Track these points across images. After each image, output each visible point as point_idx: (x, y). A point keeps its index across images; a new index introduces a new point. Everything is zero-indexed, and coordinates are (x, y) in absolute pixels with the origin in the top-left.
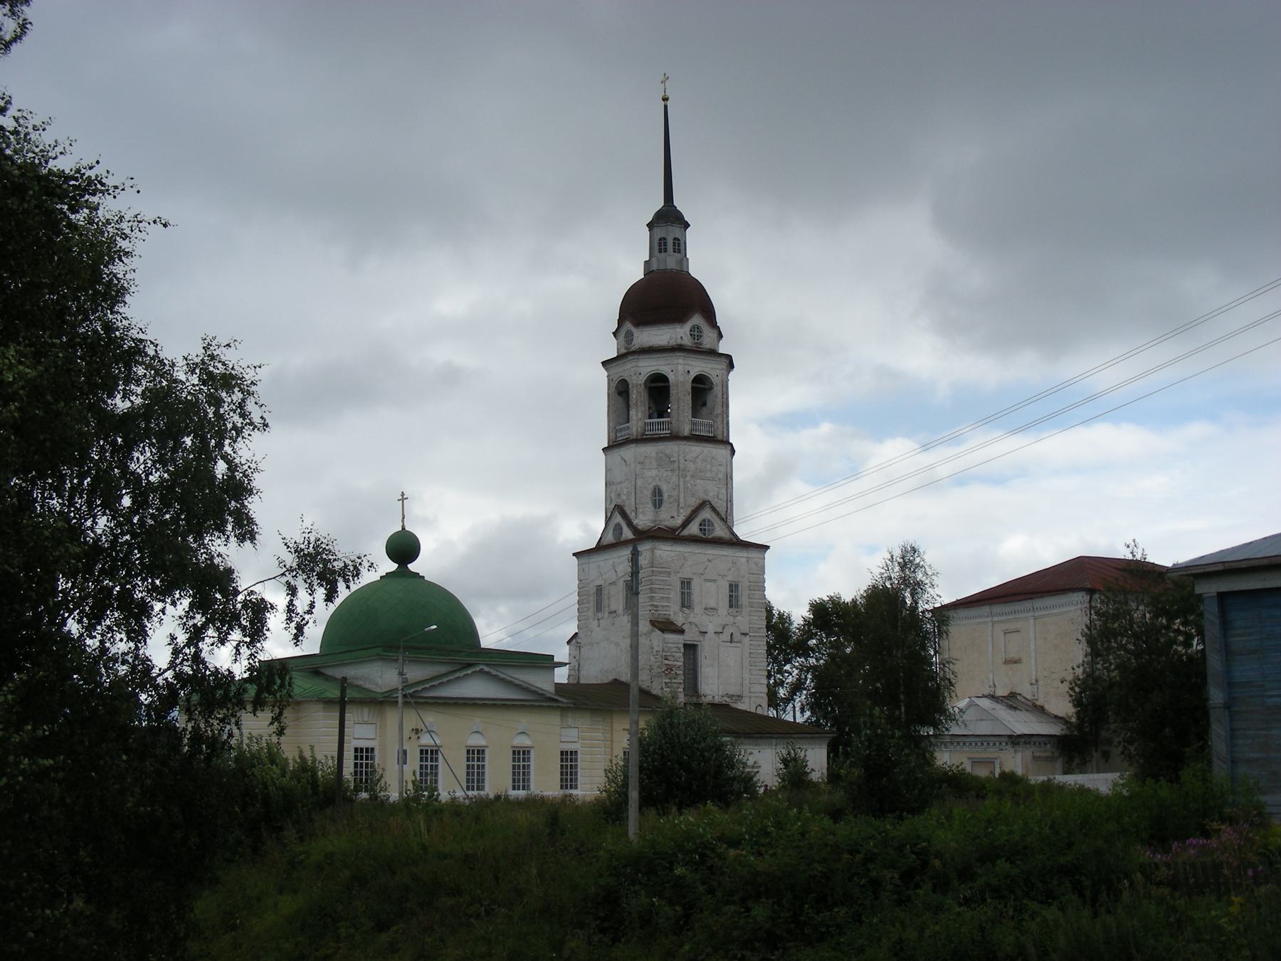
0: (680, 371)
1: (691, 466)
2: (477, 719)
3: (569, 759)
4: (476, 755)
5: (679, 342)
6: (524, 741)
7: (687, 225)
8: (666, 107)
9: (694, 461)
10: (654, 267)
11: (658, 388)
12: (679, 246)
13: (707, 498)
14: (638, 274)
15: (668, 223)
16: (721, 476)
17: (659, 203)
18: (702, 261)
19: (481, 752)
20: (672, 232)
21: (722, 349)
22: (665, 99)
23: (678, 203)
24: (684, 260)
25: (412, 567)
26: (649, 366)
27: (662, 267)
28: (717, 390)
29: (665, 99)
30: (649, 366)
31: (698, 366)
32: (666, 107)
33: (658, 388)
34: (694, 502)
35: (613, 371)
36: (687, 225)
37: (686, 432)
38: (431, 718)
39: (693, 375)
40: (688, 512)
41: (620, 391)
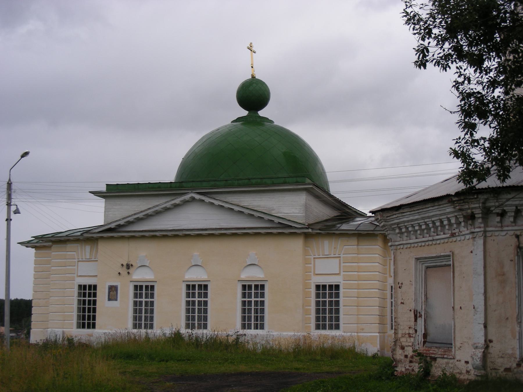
2: (197, 250)
3: (197, 293)
4: (144, 291)
6: (196, 275)
25: (262, 113)
38: (141, 252)
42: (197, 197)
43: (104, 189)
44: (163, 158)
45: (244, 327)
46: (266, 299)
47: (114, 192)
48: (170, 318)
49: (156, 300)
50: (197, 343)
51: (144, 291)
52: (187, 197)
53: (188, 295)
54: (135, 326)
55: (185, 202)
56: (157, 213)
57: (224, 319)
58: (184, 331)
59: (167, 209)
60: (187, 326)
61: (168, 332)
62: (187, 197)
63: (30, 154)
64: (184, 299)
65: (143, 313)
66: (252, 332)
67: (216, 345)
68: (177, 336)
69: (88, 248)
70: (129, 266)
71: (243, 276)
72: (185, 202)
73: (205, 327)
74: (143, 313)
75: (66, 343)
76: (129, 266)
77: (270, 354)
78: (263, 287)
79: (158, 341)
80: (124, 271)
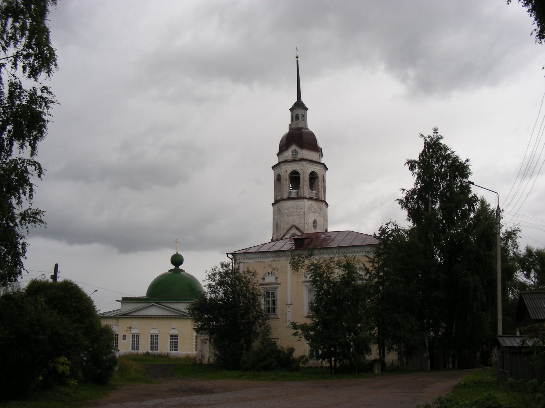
0: (305, 170)
1: (287, 211)
2: (155, 323)
3: (155, 337)
4: (136, 337)
5: (286, 159)
6: (154, 332)
7: (307, 109)
8: (297, 61)
9: (288, 209)
10: (294, 126)
11: (295, 178)
12: (304, 117)
13: (294, 224)
14: (286, 130)
15: (299, 107)
16: (301, 213)
17: (296, 100)
18: (313, 124)
19: (157, 336)
20: (300, 112)
21: (323, 161)
22: (297, 57)
23: (303, 99)
24: (306, 124)
25: (181, 267)
26: (291, 168)
27: (296, 127)
28: (320, 178)
29: (297, 57)
30: (291, 168)
31: (316, 169)
32: (297, 61)
33: (295, 178)
34: (287, 227)
35: (277, 170)
36: (307, 109)
37: (285, 197)
38: (135, 323)
39: (289, 171)
40: (285, 231)
41: (278, 179)
42: (155, 304)
43: (121, 299)
44: (141, 290)
45: (171, 350)
46: (179, 340)
47: (125, 300)
48: (145, 347)
49: (140, 340)
50: (154, 355)
51: (136, 337)
52: (151, 304)
53: (151, 339)
54: (132, 349)
55: (150, 306)
56: (140, 309)
57: (164, 348)
58: (150, 351)
59: (147, 307)
60: (151, 350)
61: (144, 351)
62: (151, 304)
63: (459, 147)
64: (150, 340)
65: (136, 344)
66: (174, 352)
67: (161, 356)
68: (148, 353)
69: (115, 321)
70: (130, 328)
71: (171, 332)
72: (150, 306)
73: (157, 350)
74: (136, 344)
75: (196, 312)
76: (130, 328)
77: (178, 359)
78: (177, 336)
79: (141, 355)
80: (128, 330)
